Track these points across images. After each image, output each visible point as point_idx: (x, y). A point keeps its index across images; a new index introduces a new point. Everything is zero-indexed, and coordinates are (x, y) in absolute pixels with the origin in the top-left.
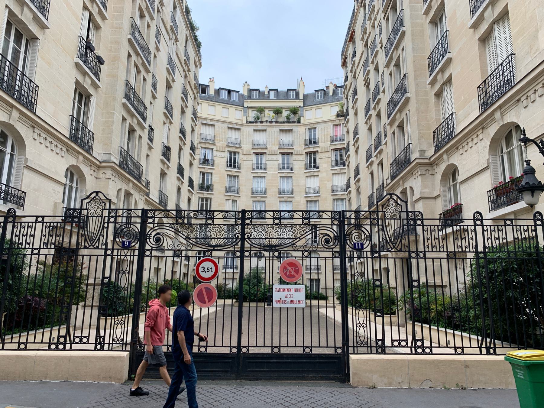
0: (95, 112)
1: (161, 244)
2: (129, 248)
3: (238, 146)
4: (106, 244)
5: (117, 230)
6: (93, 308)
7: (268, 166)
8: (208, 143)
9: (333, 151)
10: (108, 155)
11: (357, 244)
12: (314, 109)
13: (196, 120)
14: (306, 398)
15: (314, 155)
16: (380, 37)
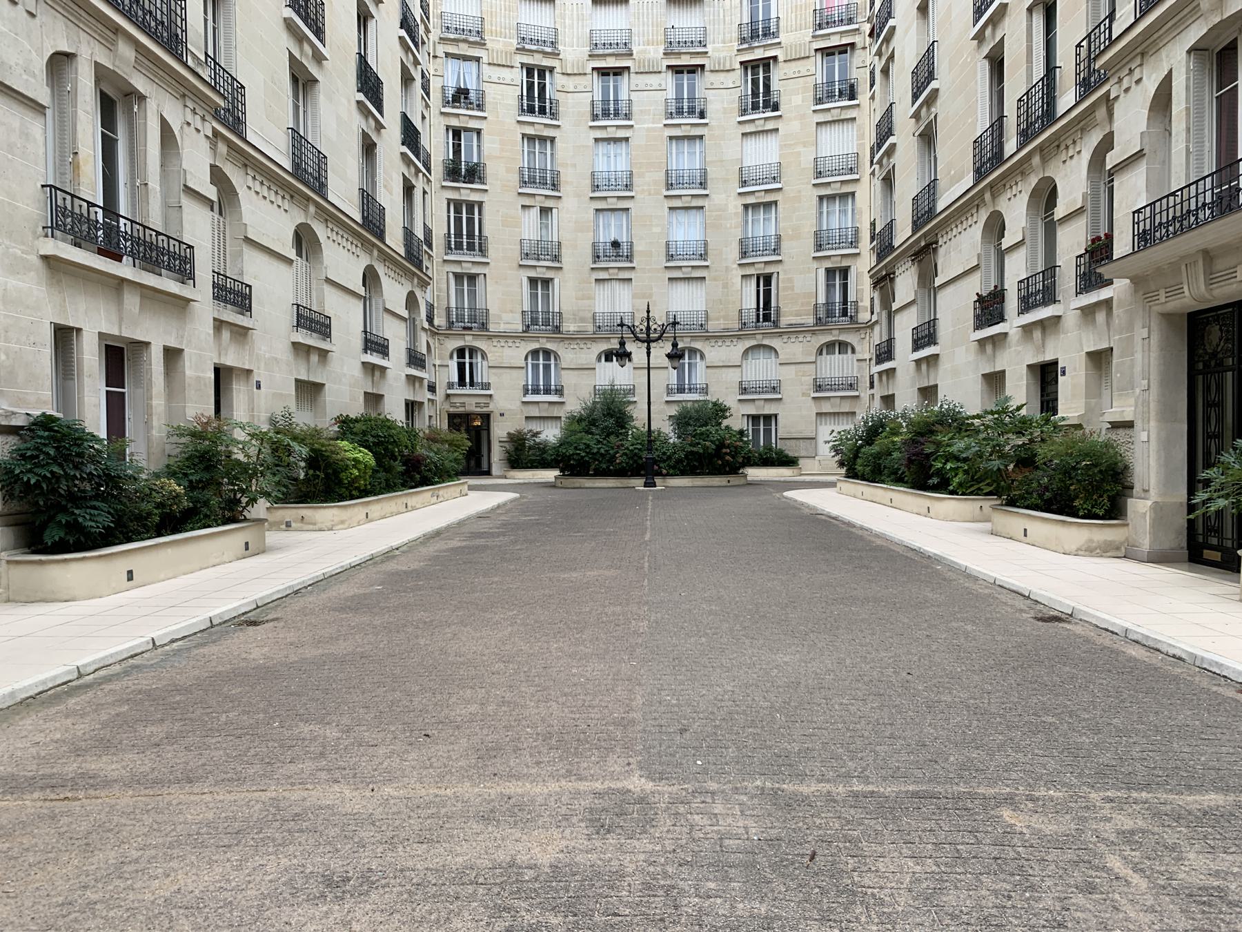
7: (635, 109)
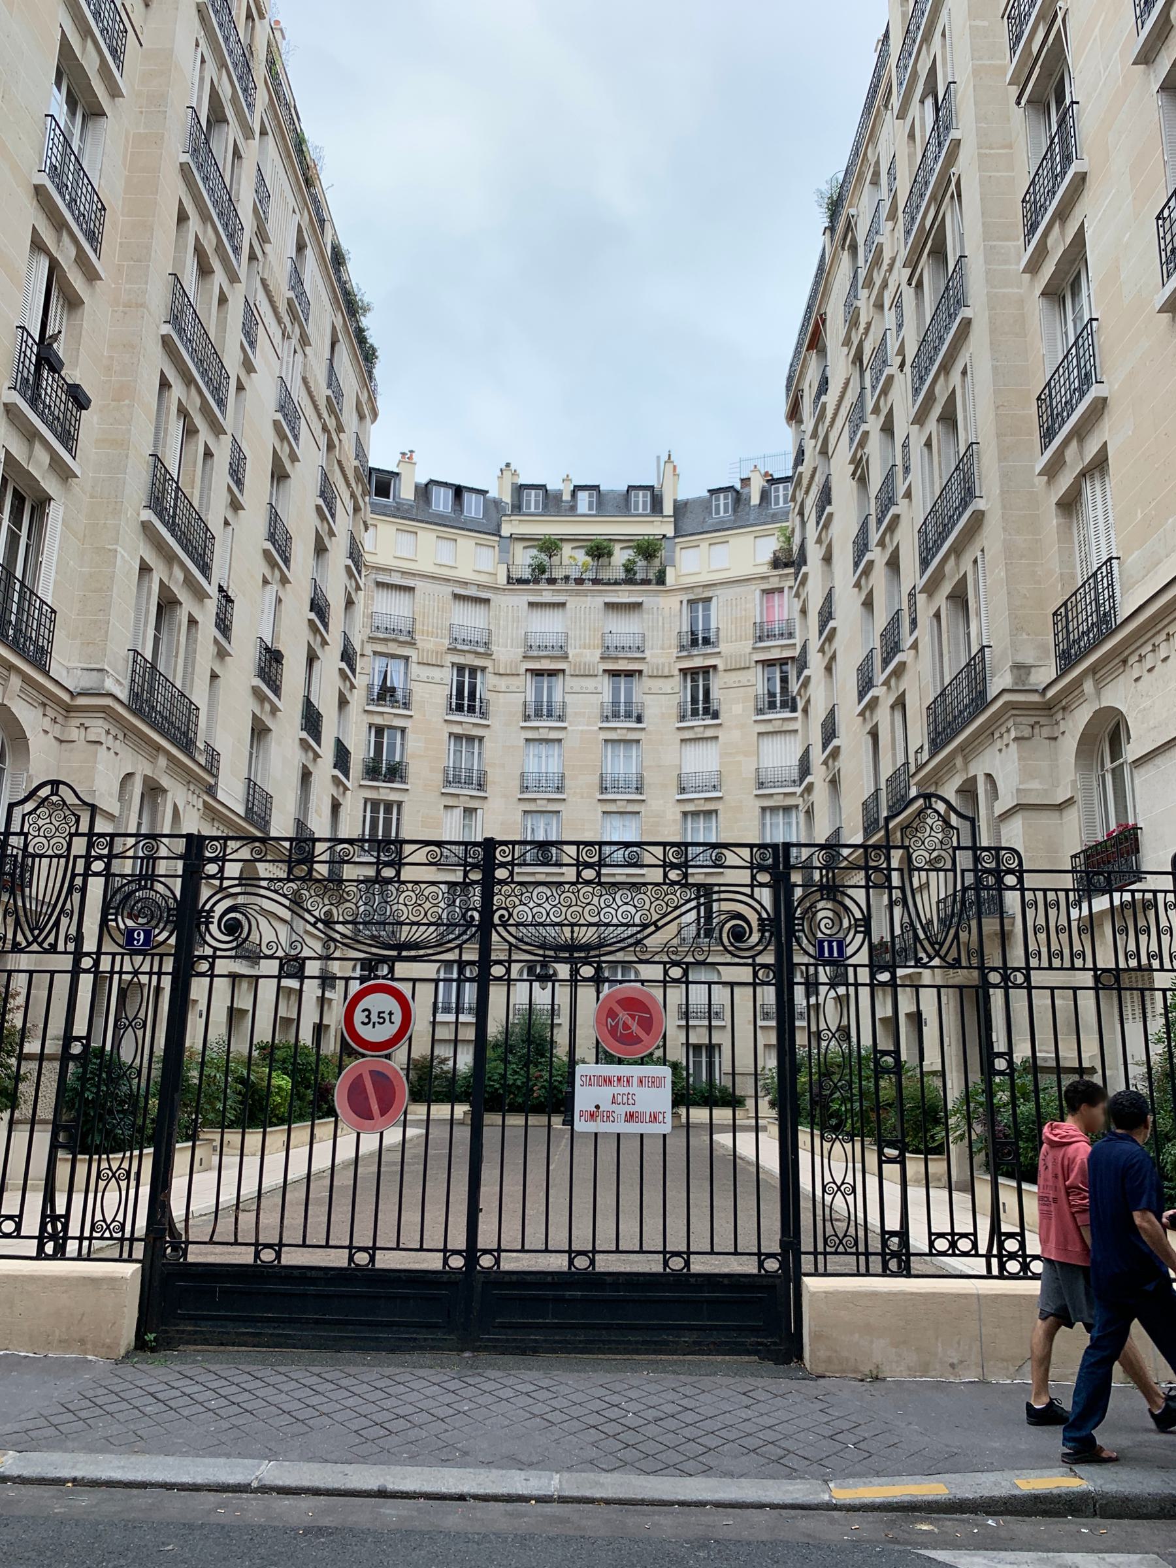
0: (61, 548)
1: (244, 935)
2: (148, 948)
3: (482, 650)
4: (79, 939)
5: (113, 896)
6: (36, 1127)
7: (569, 710)
8: (394, 640)
9: (760, 667)
10: (95, 673)
11: (826, 944)
12: (704, 546)
13: (359, 572)
14: (670, 1409)
15: (706, 679)
16: (898, 335)
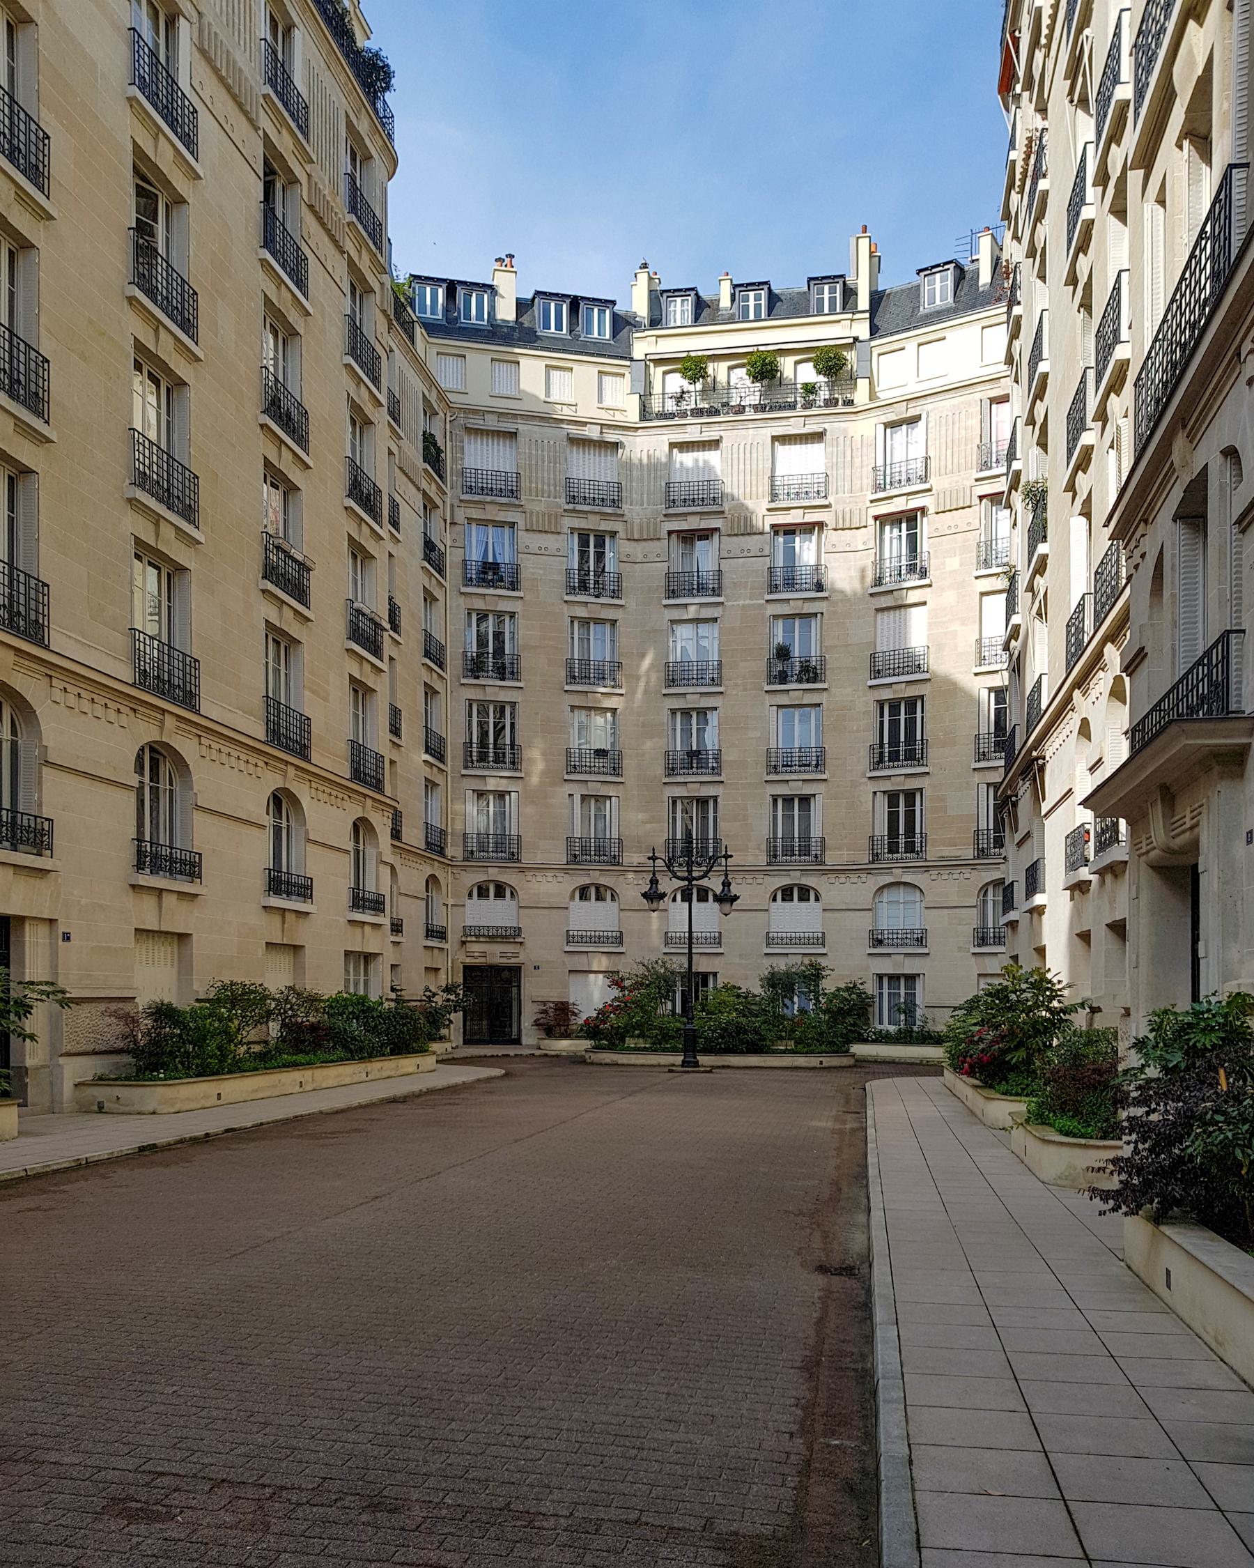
7: (726, 581)
12: (911, 346)
